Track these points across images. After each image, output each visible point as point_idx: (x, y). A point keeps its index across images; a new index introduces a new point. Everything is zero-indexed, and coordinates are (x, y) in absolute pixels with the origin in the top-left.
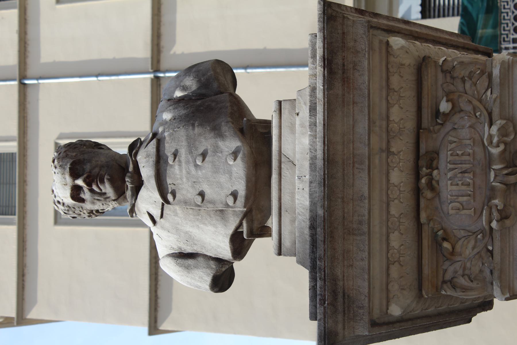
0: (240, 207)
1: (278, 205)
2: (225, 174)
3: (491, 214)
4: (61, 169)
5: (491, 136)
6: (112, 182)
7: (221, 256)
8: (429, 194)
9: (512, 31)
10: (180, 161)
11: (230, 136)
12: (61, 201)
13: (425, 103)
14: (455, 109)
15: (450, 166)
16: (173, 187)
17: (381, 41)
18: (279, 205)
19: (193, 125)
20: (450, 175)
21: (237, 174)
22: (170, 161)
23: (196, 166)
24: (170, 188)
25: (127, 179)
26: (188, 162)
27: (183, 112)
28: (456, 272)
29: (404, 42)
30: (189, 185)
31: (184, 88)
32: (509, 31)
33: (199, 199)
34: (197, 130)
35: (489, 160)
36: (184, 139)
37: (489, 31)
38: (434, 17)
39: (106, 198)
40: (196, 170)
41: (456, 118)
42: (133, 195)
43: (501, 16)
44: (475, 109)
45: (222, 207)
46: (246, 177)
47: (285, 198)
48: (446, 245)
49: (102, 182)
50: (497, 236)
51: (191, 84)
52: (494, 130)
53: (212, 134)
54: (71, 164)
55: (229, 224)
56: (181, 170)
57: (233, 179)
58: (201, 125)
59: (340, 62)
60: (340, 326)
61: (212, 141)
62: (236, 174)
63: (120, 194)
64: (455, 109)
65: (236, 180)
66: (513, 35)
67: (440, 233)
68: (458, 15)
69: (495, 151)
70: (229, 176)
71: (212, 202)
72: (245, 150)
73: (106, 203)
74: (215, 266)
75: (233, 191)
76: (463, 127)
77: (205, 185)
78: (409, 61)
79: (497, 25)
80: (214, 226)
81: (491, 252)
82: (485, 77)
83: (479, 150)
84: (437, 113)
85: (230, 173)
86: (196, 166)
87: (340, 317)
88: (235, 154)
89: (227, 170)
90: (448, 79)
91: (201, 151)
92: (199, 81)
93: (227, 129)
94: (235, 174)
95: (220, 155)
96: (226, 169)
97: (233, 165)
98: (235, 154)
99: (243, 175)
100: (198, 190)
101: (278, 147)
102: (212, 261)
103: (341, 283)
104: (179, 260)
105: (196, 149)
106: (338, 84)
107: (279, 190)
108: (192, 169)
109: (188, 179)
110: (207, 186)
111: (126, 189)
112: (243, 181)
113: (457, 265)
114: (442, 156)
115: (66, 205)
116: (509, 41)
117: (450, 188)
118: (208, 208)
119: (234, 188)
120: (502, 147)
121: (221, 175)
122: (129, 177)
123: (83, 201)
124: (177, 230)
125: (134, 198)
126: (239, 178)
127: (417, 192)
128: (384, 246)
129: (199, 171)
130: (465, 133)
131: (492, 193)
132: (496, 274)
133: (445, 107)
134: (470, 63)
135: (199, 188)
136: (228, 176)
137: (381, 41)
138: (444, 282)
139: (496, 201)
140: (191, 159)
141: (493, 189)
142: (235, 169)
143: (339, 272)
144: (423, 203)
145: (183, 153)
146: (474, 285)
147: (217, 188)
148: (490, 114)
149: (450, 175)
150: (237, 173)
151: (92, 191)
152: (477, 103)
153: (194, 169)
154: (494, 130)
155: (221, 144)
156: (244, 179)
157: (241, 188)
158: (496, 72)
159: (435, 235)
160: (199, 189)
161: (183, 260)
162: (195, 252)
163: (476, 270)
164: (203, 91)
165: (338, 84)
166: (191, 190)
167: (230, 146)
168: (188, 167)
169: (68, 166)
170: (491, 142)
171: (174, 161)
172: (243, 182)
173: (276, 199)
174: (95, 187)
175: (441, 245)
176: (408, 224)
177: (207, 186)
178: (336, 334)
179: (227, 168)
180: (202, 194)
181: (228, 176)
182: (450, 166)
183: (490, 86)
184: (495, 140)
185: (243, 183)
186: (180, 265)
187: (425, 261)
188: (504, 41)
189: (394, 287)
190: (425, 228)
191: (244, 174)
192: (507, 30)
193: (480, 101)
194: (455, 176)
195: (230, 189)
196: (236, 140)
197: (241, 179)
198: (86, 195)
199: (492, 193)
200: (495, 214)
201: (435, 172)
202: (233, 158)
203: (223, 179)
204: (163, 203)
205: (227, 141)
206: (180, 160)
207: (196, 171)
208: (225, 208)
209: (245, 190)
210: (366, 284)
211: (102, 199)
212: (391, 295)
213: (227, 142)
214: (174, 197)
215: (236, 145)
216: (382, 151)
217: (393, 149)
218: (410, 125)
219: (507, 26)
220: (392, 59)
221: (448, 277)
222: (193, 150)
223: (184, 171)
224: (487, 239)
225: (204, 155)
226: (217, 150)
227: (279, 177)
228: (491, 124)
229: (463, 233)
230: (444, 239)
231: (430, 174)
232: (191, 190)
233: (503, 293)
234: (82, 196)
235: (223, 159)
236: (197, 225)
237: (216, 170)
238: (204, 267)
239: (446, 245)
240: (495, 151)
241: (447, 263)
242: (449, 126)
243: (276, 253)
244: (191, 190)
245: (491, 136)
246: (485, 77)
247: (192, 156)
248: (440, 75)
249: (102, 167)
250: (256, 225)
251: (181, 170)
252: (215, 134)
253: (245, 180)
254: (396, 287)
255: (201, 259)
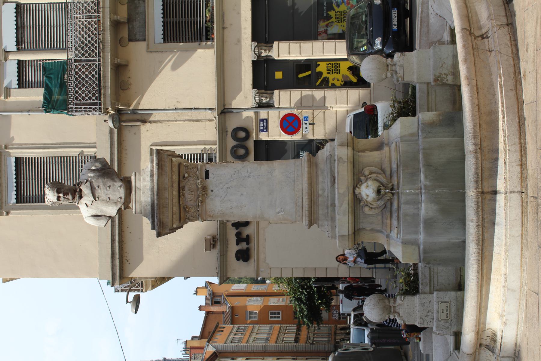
0: (123, 201)
3: (198, 201)
5: (198, 183)
6: (72, 194)
7: (111, 216)
8: (182, 197)
9: (74, 99)
10: (100, 189)
12: (51, 201)
13: (181, 174)
14: (189, 176)
15: (188, 190)
16: (98, 196)
17: (170, 159)
19: (104, 178)
20: (188, 192)
22: (97, 188)
23: (107, 190)
25: (76, 194)
26: (103, 189)
27: (98, 174)
28: (189, 216)
29: (485, 265)
31: (96, 166)
32: (73, 98)
34: (106, 180)
35: (198, 188)
36: (101, 182)
37: (61, 98)
38: (26, 88)
41: (189, 178)
42: (154, 201)
43: (68, 90)
44: (194, 176)
47: (138, 199)
48: (187, 209)
49: (68, 195)
50: (200, 207)
52: (199, 181)
53: (112, 181)
54: (57, 189)
56: (101, 191)
58: (107, 178)
59: (161, 164)
60: (162, 231)
61: (112, 183)
63: (74, 198)
64: (189, 176)
66: (75, 101)
67: (185, 206)
68: (43, 87)
69: (200, 186)
72: (123, 185)
76: (191, 180)
78: (177, 164)
79: (66, 94)
80: (113, 207)
81: (199, 211)
82: (196, 168)
83: (195, 186)
84: (184, 177)
85: (119, 192)
86: (107, 190)
87: (162, 228)
88: (121, 186)
90: (187, 168)
91: (108, 185)
92: (102, 165)
93: (116, 179)
98: (121, 186)
103: (162, 220)
105: (106, 185)
106: (160, 170)
108: (106, 191)
109: (104, 194)
113: (190, 214)
114: (186, 187)
116: (73, 104)
117: (188, 195)
120: (201, 185)
123: (60, 200)
124: (97, 208)
127: (179, 196)
128: (171, 210)
130: (191, 182)
131: (199, 197)
132: (200, 216)
133: (186, 175)
134: (192, 165)
137: (170, 159)
138: (186, 218)
139: (200, 198)
141: (199, 195)
142: (120, 191)
143: (161, 217)
144: (181, 199)
145: (101, 186)
146: (194, 219)
148: (198, 178)
149: (188, 192)
151: (64, 197)
152: (194, 175)
154: (199, 181)
155: (115, 184)
157: (123, 196)
158: (199, 167)
159: (184, 207)
163: (194, 215)
164: (104, 168)
165: (160, 170)
166: (105, 197)
169: (56, 190)
170: (198, 184)
174: (65, 196)
175: (186, 209)
176: (177, 204)
178: (161, 233)
180: (109, 198)
182: (188, 190)
183: (198, 170)
184: (199, 184)
187: (181, 214)
188: (70, 104)
189: (174, 220)
190: (181, 206)
192: (72, 98)
193: (195, 174)
194: (189, 192)
198: (62, 199)
199: (199, 197)
200: (200, 201)
201: (184, 191)
203: (117, 194)
210: (168, 220)
212: (173, 222)
214: (99, 199)
216: (170, 186)
217: (174, 186)
218: (177, 180)
219: (72, 96)
220: (172, 163)
221: (187, 217)
223: (102, 191)
224: (197, 208)
225: (109, 187)
226: (114, 185)
228: (198, 180)
229: (191, 206)
230: (186, 208)
231: (183, 192)
233: (201, 220)
234: (60, 199)
237: (114, 191)
239: (187, 209)
240: (200, 186)
241: (187, 214)
242: (187, 180)
245: (198, 183)
246: (196, 168)
248: (184, 167)
249: (67, 190)
250: (126, 206)
251: (101, 191)
254: (175, 220)
255: (103, 217)
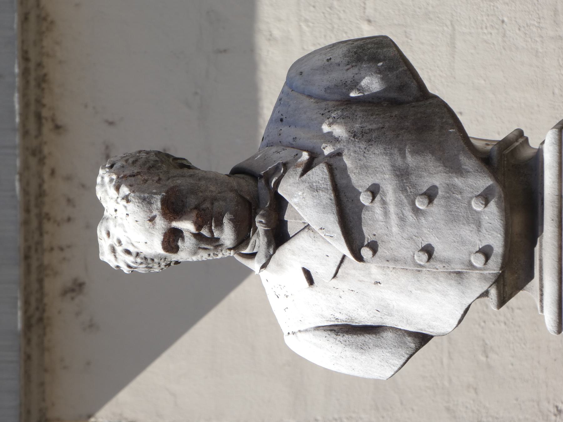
1: (557, 268)
2: (469, 223)
4: (142, 204)
11: (474, 172)
18: (558, 267)
21: (490, 225)
24: (368, 236)
30: (402, 237)
33: (425, 257)
39: (216, 247)
40: (415, 216)
45: (462, 269)
46: (504, 229)
49: (220, 224)
51: (369, 81)
55: (469, 291)
57: (482, 231)
62: (487, 225)
65: (487, 233)
70: (475, 228)
71: (447, 262)
73: (215, 253)
74: (415, 344)
75: (482, 248)
77: (433, 238)
86: (416, 211)
88: (485, 197)
89: (473, 218)
94: (486, 223)
95: (459, 197)
96: (470, 216)
97: (481, 211)
99: (499, 227)
100: (420, 244)
101: (557, 190)
102: (409, 337)
104: (347, 336)
107: (559, 247)
110: (437, 239)
111: (252, 233)
112: (500, 234)
115: (142, 255)
118: (437, 269)
119: (484, 243)
121: (462, 225)
122: (263, 216)
125: (272, 248)
126: (494, 230)
129: (422, 218)
135: (423, 242)
136: (474, 227)
140: (405, 201)
142: (485, 218)
147: (455, 242)
150: (490, 224)
153: (411, 214)
156: (502, 232)
160: (422, 243)
161: (355, 336)
162: (380, 324)
167: (476, 186)
168: (402, 211)
171: (372, 202)
172: (499, 235)
173: (554, 260)
177: (438, 240)
179: (472, 215)
180: (428, 251)
181: (474, 227)
185: (499, 237)
186: (348, 343)
191: (502, 225)
195: (476, 244)
196: (485, 177)
197: (497, 232)
202: (484, 203)
204: (344, 257)
205: (469, 178)
206: (384, 201)
207: (416, 218)
208: (467, 269)
209: (502, 246)
211: (212, 248)
213: (469, 179)
215: (485, 183)
222: (408, 188)
227: (558, 231)
232: (406, 244)
235: (465, 203)
236: (408, 291)
238: (395, 346)
243: (554, 332)
244: (406, 244)
247: (407, 196)
252: (446, 167)
253: (502, 233)
